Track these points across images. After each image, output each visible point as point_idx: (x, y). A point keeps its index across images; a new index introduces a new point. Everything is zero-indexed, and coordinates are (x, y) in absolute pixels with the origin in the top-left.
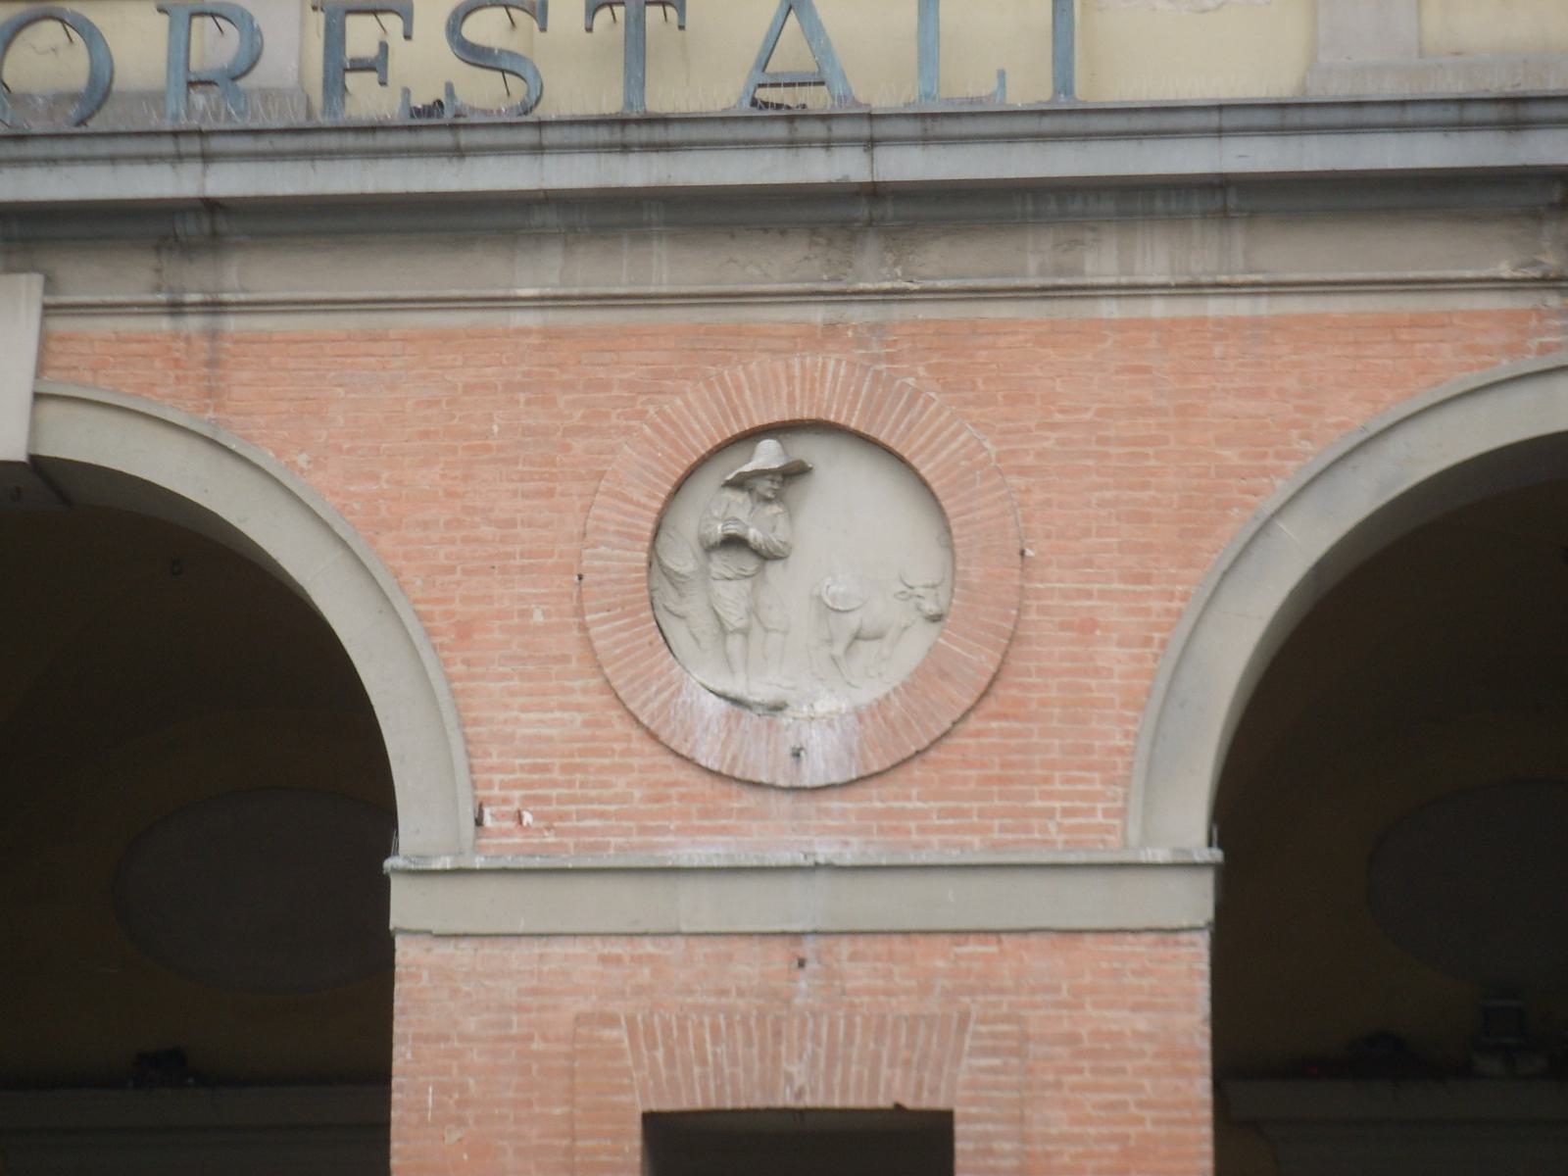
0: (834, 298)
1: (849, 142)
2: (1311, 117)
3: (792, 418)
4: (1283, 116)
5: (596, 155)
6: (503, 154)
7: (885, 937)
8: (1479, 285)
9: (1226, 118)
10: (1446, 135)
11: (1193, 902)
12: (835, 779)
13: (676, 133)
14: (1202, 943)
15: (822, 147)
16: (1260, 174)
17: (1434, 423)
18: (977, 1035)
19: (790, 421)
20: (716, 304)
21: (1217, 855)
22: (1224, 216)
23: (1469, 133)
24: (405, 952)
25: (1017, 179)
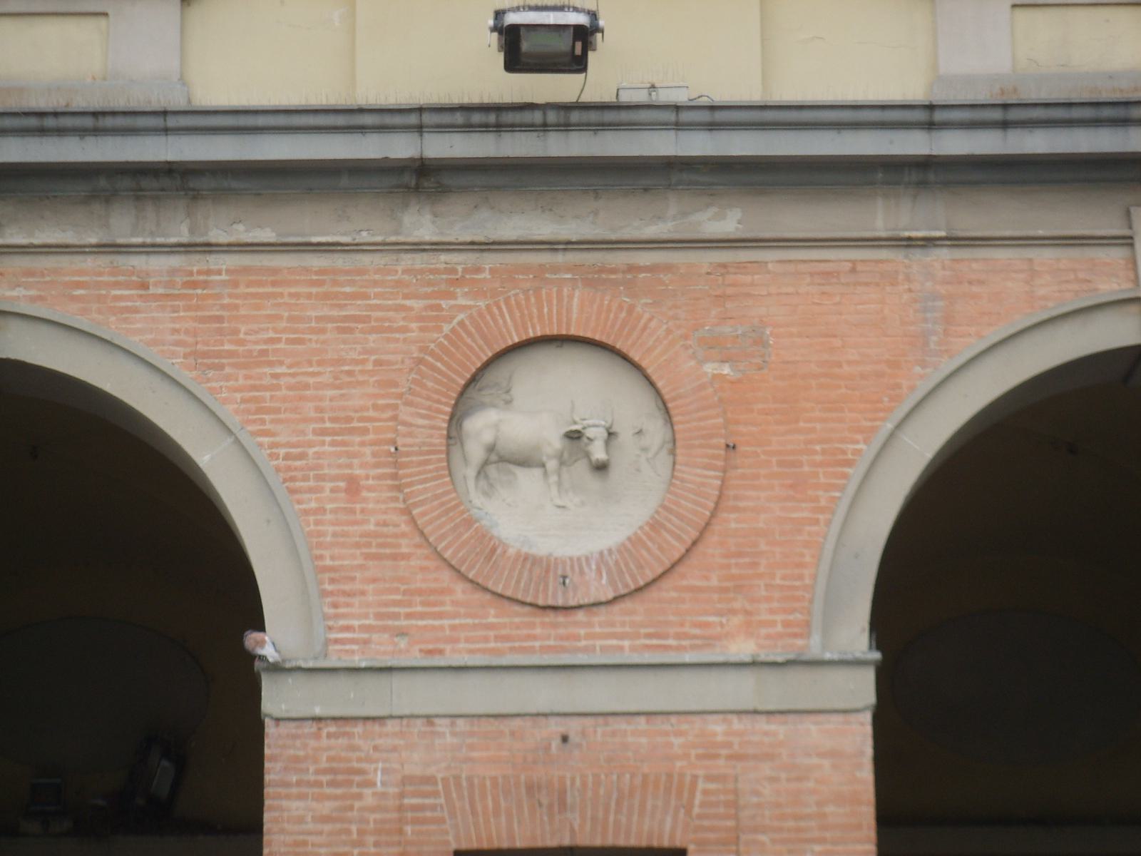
0: (860, 243)
1: (401, 128)
2: (368, 120)
3: (544, 334)
4: (929, 116)
5: (94, 138)
6: (1073, 126)
7: (749, 716)
8: (1072, 242)
9: (418, 118)
10: (839, 133)
11: (861, 689)
12: (603, 599)
13: (341, 120)
14: (867, 717)
15: (417, 132)
16: (1106, 154)
17: (1025, 343)
18: (705, 792)
19: (557, 335)
20: (798, 247)
21: (877, 655)
22: (922, 184)
23: (1100, 128)
24: (270, 729)
25: (181, 162)
